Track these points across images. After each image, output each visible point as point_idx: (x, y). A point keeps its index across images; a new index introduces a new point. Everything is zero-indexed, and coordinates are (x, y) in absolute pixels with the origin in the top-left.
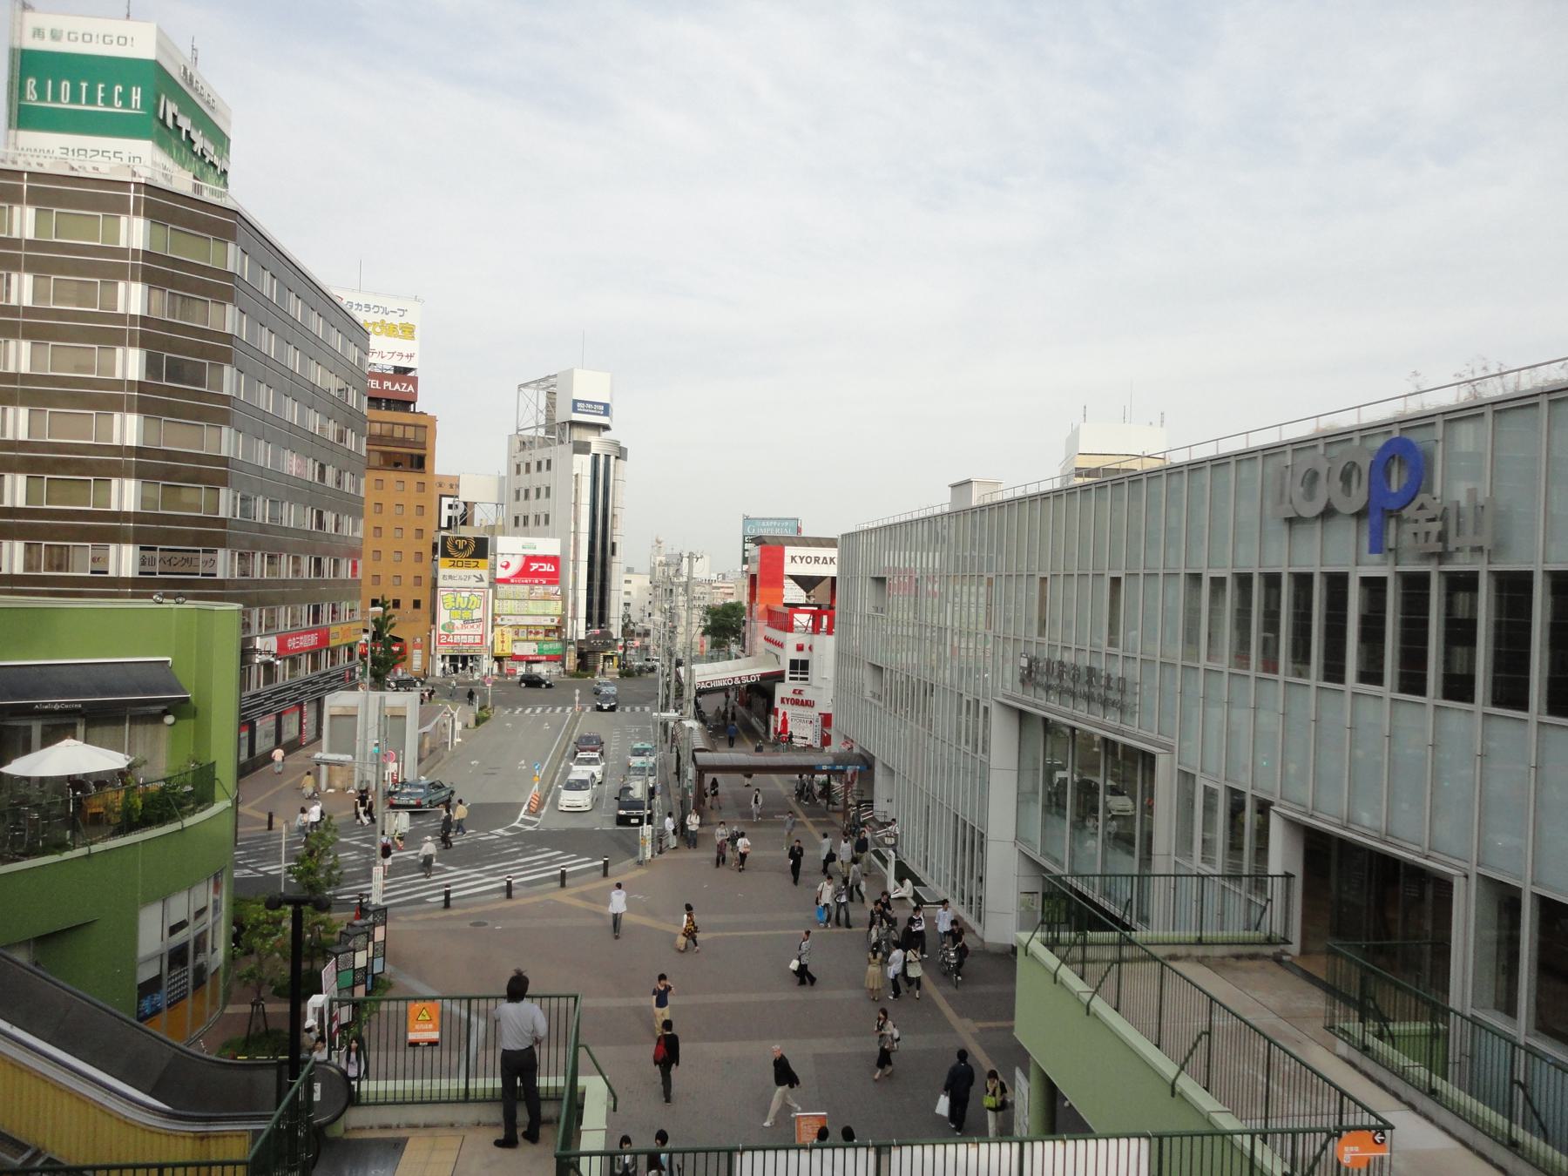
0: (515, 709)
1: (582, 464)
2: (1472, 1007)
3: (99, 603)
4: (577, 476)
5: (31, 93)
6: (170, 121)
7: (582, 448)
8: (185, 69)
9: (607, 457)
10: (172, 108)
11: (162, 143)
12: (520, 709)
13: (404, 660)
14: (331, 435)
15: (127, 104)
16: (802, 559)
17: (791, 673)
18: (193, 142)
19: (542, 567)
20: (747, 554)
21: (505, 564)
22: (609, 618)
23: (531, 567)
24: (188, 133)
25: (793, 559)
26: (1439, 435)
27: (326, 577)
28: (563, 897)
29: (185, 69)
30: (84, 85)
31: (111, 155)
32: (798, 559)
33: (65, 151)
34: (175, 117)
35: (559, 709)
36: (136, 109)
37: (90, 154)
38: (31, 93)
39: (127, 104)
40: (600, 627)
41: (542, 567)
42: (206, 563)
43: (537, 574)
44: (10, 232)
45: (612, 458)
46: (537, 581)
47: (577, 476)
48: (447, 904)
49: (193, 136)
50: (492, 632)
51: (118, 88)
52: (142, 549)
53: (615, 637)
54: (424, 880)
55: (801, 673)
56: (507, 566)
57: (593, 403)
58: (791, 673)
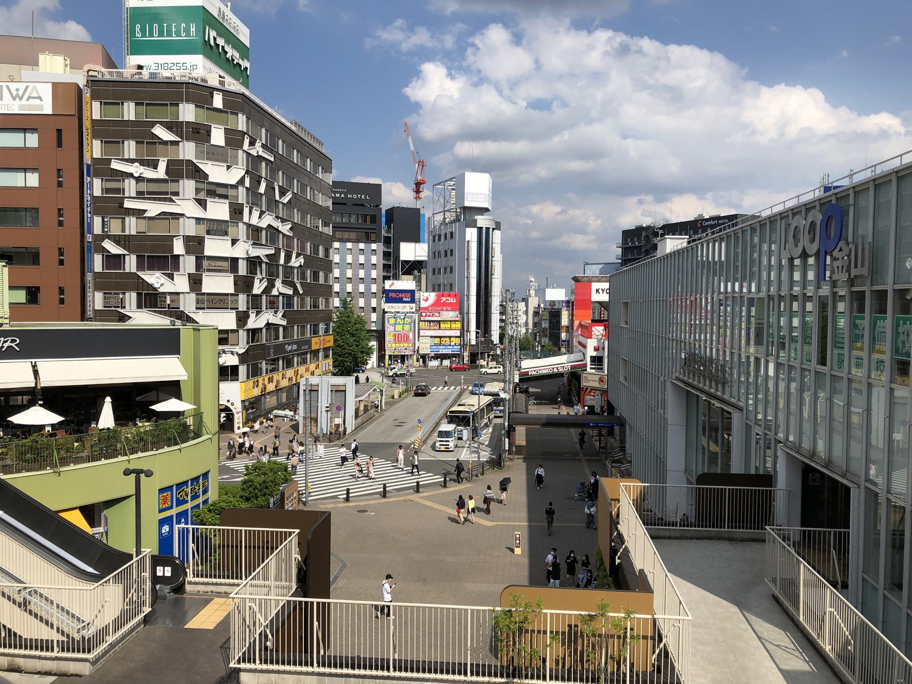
0: (438, 387)
1: (471, 234)
2: (863, 572)
3: (46, 325)
4: (468, 241)
5: (138, 33)
6: (212, 43)
7: (473, 224)
8: (220, 9)
9: (488, 229)
10: (213, 34)
11: (208, 56)
12: (454, 387)
13: (901, 374)
14: (348, 221)
15: (188, 34)
16: (603, 291)
17: (591, 365)
18: (226, 53)
19: (449, 300)
20: (181, 295)
21: (425, 298)
22: (490, 331)
23: (442, 300)
24: (223, 47)
25: (597, 291)
26: (851, 201)
27: (296, 309)
28: (415, 497)
29: (220, 9)
30: (165, 25)
31: (181, 65)
32: (600, 291)
33: (157, 65)
34: (215, 39)
35: (453, 387)
36: (193, 37)
37: (170, 65)
38: (138, 33)
39: (188, 34)
40: (485, 337)
41: (449, 300)
42: (232, 301)
43: (444, 304)
44: (123, 117)
45: (491, 230)
46: (445, 309)
47: (468, 241)
48: (347, 499)
49: (226, 48)
50: (419, 340)
51: (183, 25)
52: (104, 293)
53: (495, 343)
54: (349, 487)
55: (598, 365)
56: (427, 300)
57: (478, 194)
58: (591, 365)
